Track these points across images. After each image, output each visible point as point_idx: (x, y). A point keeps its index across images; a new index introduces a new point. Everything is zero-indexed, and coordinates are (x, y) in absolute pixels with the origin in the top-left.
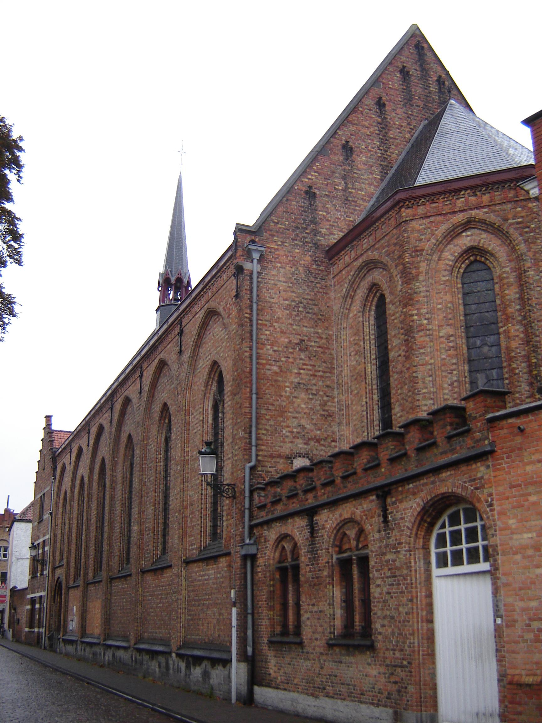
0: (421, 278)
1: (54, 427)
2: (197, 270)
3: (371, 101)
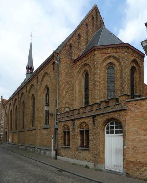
0: (98, 69)
1: (3, 99)
2: (36, 66)
3: (84, 24)
